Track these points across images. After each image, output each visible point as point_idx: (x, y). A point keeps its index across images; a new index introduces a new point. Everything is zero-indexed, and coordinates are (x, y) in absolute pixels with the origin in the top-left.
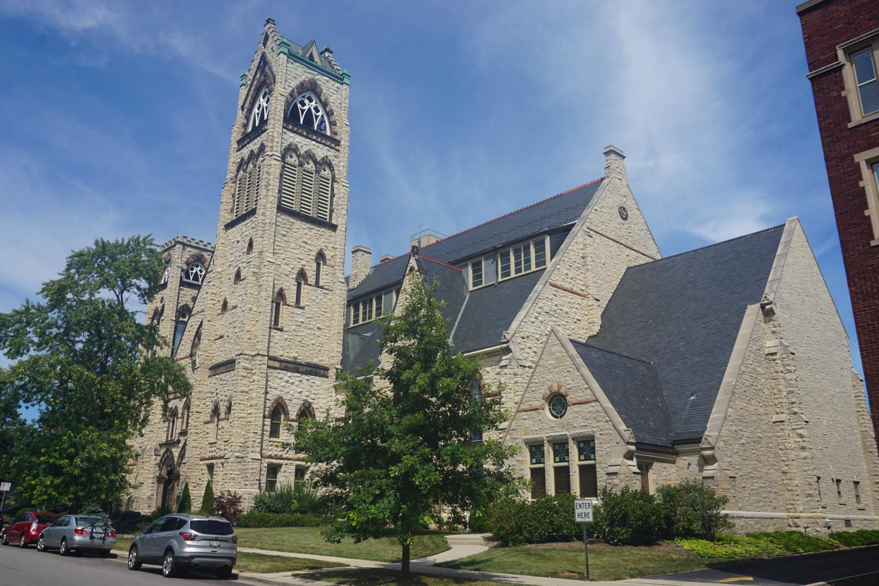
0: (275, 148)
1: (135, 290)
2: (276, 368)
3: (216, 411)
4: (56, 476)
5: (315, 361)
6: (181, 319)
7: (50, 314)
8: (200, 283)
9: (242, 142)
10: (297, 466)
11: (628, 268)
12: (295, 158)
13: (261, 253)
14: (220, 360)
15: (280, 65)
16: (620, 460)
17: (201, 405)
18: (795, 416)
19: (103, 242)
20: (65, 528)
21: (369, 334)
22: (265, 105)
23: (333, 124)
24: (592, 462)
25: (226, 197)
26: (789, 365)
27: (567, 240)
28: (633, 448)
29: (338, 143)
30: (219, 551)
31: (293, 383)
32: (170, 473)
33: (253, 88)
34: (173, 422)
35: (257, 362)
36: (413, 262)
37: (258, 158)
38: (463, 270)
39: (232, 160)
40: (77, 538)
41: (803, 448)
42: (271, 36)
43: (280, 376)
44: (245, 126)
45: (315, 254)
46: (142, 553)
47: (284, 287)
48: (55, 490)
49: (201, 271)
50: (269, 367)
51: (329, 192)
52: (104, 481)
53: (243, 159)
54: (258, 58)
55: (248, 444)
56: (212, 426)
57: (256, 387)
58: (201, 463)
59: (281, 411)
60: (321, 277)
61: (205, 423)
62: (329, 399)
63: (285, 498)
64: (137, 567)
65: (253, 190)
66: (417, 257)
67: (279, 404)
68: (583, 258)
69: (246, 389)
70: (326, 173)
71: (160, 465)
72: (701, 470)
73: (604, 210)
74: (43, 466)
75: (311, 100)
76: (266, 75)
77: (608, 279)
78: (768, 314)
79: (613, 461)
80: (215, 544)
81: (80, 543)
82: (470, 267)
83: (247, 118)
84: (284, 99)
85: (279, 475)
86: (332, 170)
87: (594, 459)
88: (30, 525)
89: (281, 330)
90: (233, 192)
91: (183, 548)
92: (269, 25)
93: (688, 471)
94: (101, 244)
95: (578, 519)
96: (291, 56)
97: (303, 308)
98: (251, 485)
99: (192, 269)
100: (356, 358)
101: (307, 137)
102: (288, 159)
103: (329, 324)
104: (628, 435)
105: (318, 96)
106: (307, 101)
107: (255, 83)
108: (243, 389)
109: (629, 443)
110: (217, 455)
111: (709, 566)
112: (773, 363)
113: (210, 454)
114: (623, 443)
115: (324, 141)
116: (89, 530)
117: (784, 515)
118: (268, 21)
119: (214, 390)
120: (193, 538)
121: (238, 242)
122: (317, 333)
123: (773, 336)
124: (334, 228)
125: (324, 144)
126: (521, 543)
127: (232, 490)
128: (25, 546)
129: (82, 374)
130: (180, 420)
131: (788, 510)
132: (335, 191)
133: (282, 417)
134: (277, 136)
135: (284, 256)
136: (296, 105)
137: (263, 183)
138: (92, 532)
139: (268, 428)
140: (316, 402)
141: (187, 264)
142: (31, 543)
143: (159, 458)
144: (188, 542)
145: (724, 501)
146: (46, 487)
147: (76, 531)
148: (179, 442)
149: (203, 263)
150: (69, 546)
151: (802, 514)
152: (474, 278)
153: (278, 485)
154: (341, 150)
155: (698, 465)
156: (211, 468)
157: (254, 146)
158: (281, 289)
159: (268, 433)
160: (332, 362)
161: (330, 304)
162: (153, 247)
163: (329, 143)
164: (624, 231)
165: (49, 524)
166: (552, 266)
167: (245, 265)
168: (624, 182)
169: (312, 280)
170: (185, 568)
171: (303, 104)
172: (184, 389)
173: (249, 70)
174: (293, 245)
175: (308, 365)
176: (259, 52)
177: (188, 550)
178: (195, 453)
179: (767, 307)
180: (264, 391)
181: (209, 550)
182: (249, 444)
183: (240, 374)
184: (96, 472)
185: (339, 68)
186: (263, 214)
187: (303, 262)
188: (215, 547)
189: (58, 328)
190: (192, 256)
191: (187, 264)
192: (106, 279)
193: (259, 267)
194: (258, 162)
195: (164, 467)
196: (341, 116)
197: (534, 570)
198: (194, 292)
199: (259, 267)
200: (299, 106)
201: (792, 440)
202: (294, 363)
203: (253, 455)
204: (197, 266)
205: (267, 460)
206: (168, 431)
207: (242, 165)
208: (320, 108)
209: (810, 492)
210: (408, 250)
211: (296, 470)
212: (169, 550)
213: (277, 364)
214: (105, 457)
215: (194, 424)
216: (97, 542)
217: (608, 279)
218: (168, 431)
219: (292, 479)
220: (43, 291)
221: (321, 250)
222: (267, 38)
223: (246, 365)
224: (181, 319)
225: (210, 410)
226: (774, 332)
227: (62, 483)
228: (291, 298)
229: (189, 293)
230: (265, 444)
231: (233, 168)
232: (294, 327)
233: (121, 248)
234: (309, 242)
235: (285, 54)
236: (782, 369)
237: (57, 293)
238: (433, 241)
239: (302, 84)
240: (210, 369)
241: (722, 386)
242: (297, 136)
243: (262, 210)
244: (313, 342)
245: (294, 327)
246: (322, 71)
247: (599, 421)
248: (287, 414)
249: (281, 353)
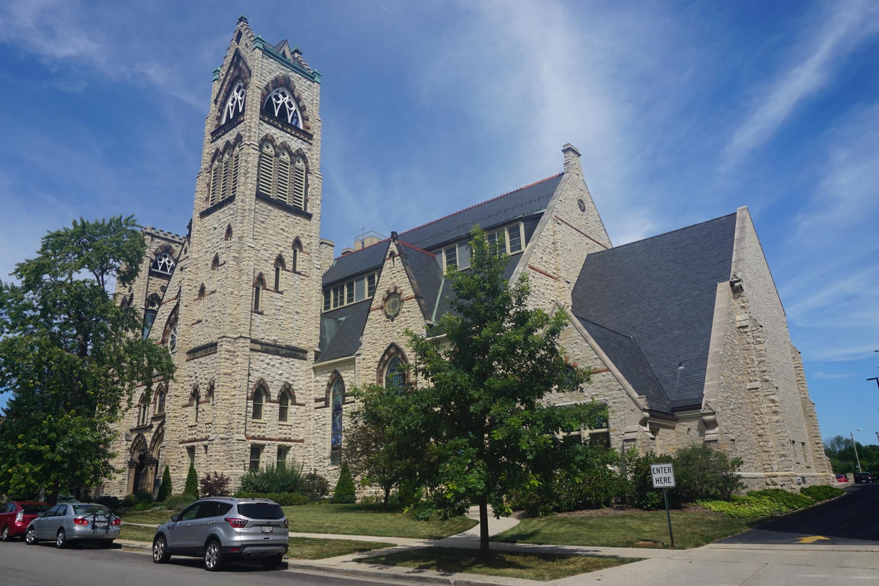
0: (253, 138)
1: (115, 273)
2: (257, 351)
3: (195, 395)
4: (34, 463)
5: (294, 344)
6: (150, 308)
7: (26, 296)
8: (168, 273)
9: (217, 134)
10: (279, 446)
11: (588, 255)
12: (271, 148)
13: (240, 238)
14: (199, 344)
15: (255, 60)
16: (637, 426)
17: (178, 391)
18: (766, 384)
19: (83, 222)
20: (62, 517)
21: (343, 319)
22: (240, 98)
23: (305, 119)
24: (605, 430)
25: (201, 186)
26: (759, 337)
27: (538, 227)
28: (647, 414)
29: (310, 136)
30: (271, 538)
31: (274, 366)
32: (141, 458)
33: (226, 83)
34: (145, 408)
35: (240, 344)
36: (393, 247)
37: (234, 148)
38: (437, 257)
39: (206, 150)
40: (78, 528)
41: (775, 412)
42: (244, 33)
43: (261, 358)
44: (219, 119)
45: (292, 241)
46: (171, 544)
47: (264, 272)
48: (33, 478)
49: (169, 262)
50: (251, 350)
51: (303, 183)
52: (88, 466)
53: (218, 149)
54: (231, 55)
55: (233, 425)
56: (191, 410)
57: (239, 369)
58: (181, 446)
59: (263, 393)
60: (298, 263)
61: (184, 407)
62: (308, 381)
63: (269, 476)
64: (165, 559)
65: (230, 179)
66: (397, 242)
67: (261, 386)
68: (553, 243)
69: (229, 371)
70: (301, 164)
71: (132, 450)
72: (702, 434)
73: (567, 202)
74: (20, 453)
75: (284, 96)
76: (240, 70)
77: (573, 264)
78: (737, 290)
79: (629, 428)
80: (267, 529)
81: (80, 533)
82: (443, 254)
83: (221, 111)
84: (260, 92)
85: (262, 455)
86: (306, 162)
87: (607, 427)
88: (14, 516)
89: (261, 313)
90: (207, 181)
91: (232, 536)
92: (242, 23)
93: (688, 436)
94: (79, 224)
95: (656, 485)
96: (266, 52)
97: (281, 293)
98: (237, 466)
99: (161, 260)
100: (332, 341)
101: (282, 130)
102: (265, 150)
103: (306, 309)
104: (643, 402)
105: (292, 92)
106: (281, 96)
107: (229, 77)
108: (226, 371)
109: (644, 410)
110: (199, 437)
111: (750, 525)
112: (745, 336)
113: (190, 437)
114: (638, 410)
115: (298, 135)
116: (90, 519)
117: (762, 474)
118: (241, 19)
119: (192, 374)
120: (242, 524)
121: (215, 229)
122: (296, 317)
123: (742, 311)
124: (309, 217)
125: (298, 137)
126: (551, 512)
127: (219, 472)
128: (10, 539)
129: (62, 355)
130: (152, 406)
131: (765, 470)
132: (310, 182)
133: (264, 398)
134: (254, 127)
135: (262, 242)
136: (270, 98)
137: (242, 171)
138: (94, 521)
139: (251, 409)
140: (295, 383)
141: (156, 254)
142: (18, 536)
143: (130, 443)
144: (238, 530)
145: (738, 463)
146: (24, 474)
147: (76, 521)
148: (151, 426)
149: (171, 254)
150: (67, 538)
151: (778, 473)
152: (448, 263)
153: (261, 465)
154: (314, 143)
155: (698, 430)
156: (191, 451)
157: (230, 136)
158: (261, 274)
159: (251, 415)
160: (311, 345)
161: (307, 289)
162: (135, 228)
163: (302, 137)
164: (583, 222)
165: (40, 514)
166: (529, 250)
167: (223, 251)
168: (581, 178)
169: (289, 266)
170: (234, 560)
171: (278, 99)
172: (168, 371)
173: (222, 66)
174: (271, 232)
175: (288, 348)
176: (232, 49)
177: (237, 538)
178: (174, 436)
179: (736, 284)
180: (247, 373)
181: (261, 537)
182: (234, 425)
183: (223, 356)
184: (79, 458)
185: (309, 67)
186: (243, 201)
187: (281, 249)
188: (267, 533)
189: (35, 309)
190: (160, 247)
191: (156, 254)
192: (88, 258)
193: (239, 252)
194: (235, 153)
195: (136, 452)
196: (313, 111)
197: (605, 542)
198: (164, 282)
199: (239, 252)
200: (274, 99)
201: (764, 405)
202: (275, 346)
203: (238, 437)
204: (165, 257)
205: (251, 441)
206: (139, 416)
207: (217, 155)
208: (293, 103)
209: (783, 452)
210: (389, 236)
211: (279, 450)
212: (213, 539)
213: (258, 347)
214: (89, 442)
215: (172, 407)
216: (100, 532)
217: (573, 264)
218: (139, 416)
219: (275, 458)
220: (15, 273)
221: (297, 237)
222: (240, 35)
223: (229, 348)
224: (150, 308)
225: (189, 394)
226: (743, 307)
227: (41, 470)
228: (270, 284)
229: (159, 282)
230: (248, 425)
231: (208, 159)
232: (274, 311)
233: (103, 229)
234: (286, 229)
235: (260, 49)
236: (753, 341)
237: (32, 273)
238: (376, 241)
239: (276, 79)
240: (187, 353)
241: (710, 356)
242: (273, 128)
243: (241, 197)
244: (292, 325)
245: (274, 311)
246: (299, 69)
247: (611, 390)
248: (268, 395)
249: (262, 336)
